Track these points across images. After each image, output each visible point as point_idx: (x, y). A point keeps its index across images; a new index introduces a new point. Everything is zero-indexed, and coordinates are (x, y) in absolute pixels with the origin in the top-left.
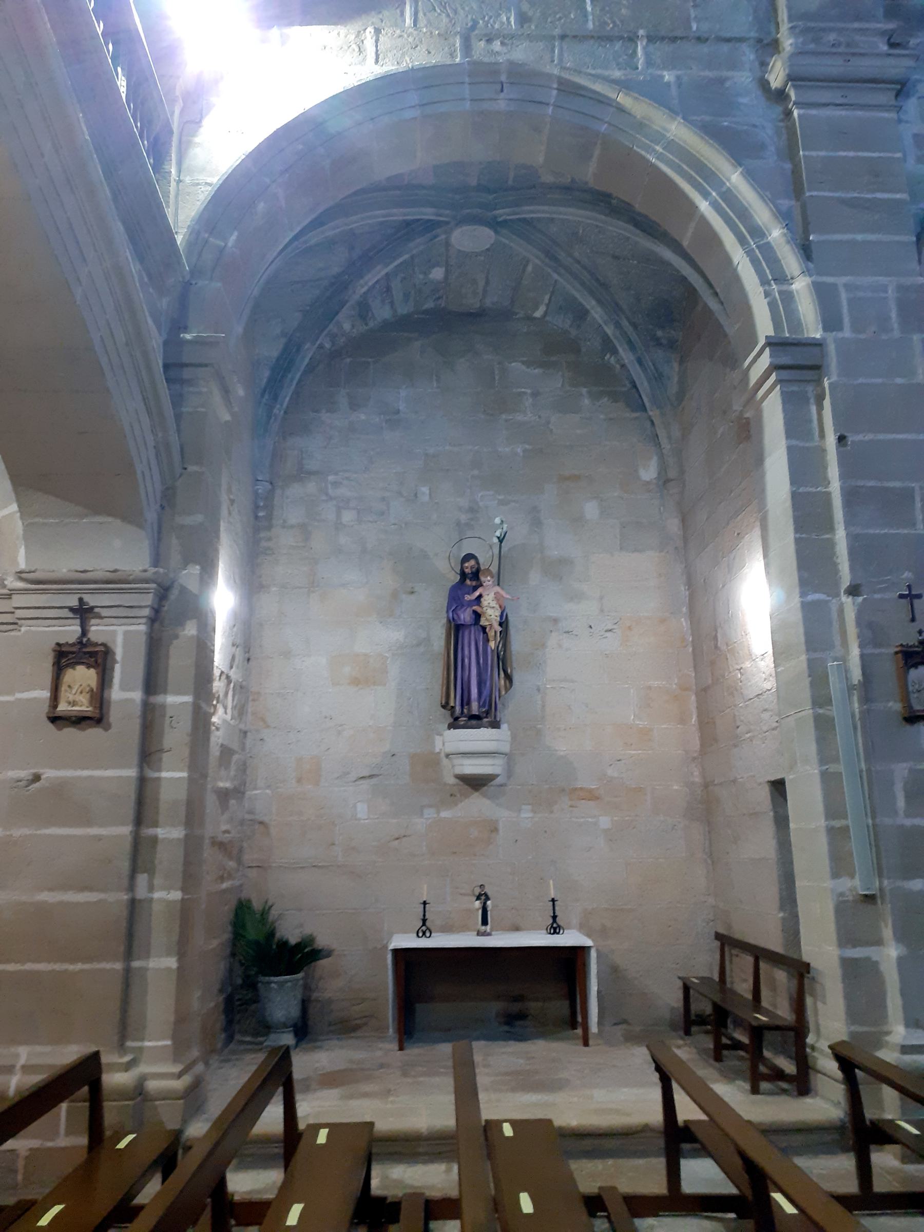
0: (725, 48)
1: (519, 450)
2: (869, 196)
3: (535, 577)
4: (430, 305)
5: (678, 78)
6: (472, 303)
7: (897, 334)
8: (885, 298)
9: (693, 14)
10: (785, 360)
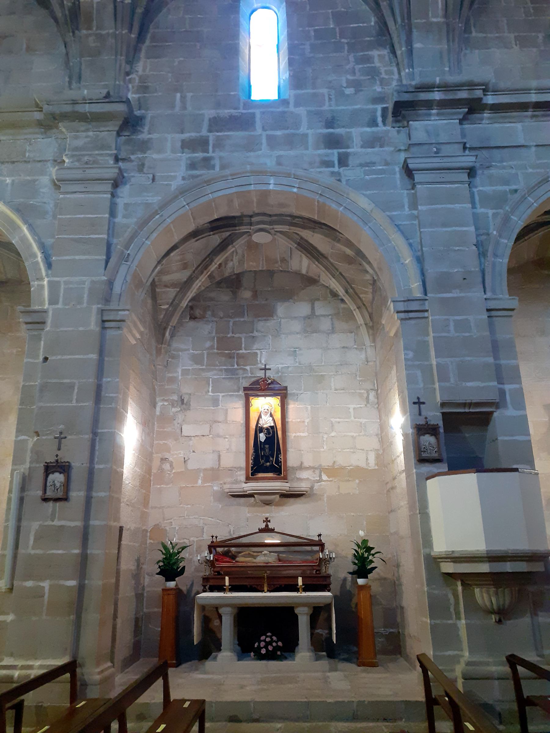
0: (39, 165)
2: (87, 237)
5: (13, 181)
7: (85, 305)
9: (28, 148)
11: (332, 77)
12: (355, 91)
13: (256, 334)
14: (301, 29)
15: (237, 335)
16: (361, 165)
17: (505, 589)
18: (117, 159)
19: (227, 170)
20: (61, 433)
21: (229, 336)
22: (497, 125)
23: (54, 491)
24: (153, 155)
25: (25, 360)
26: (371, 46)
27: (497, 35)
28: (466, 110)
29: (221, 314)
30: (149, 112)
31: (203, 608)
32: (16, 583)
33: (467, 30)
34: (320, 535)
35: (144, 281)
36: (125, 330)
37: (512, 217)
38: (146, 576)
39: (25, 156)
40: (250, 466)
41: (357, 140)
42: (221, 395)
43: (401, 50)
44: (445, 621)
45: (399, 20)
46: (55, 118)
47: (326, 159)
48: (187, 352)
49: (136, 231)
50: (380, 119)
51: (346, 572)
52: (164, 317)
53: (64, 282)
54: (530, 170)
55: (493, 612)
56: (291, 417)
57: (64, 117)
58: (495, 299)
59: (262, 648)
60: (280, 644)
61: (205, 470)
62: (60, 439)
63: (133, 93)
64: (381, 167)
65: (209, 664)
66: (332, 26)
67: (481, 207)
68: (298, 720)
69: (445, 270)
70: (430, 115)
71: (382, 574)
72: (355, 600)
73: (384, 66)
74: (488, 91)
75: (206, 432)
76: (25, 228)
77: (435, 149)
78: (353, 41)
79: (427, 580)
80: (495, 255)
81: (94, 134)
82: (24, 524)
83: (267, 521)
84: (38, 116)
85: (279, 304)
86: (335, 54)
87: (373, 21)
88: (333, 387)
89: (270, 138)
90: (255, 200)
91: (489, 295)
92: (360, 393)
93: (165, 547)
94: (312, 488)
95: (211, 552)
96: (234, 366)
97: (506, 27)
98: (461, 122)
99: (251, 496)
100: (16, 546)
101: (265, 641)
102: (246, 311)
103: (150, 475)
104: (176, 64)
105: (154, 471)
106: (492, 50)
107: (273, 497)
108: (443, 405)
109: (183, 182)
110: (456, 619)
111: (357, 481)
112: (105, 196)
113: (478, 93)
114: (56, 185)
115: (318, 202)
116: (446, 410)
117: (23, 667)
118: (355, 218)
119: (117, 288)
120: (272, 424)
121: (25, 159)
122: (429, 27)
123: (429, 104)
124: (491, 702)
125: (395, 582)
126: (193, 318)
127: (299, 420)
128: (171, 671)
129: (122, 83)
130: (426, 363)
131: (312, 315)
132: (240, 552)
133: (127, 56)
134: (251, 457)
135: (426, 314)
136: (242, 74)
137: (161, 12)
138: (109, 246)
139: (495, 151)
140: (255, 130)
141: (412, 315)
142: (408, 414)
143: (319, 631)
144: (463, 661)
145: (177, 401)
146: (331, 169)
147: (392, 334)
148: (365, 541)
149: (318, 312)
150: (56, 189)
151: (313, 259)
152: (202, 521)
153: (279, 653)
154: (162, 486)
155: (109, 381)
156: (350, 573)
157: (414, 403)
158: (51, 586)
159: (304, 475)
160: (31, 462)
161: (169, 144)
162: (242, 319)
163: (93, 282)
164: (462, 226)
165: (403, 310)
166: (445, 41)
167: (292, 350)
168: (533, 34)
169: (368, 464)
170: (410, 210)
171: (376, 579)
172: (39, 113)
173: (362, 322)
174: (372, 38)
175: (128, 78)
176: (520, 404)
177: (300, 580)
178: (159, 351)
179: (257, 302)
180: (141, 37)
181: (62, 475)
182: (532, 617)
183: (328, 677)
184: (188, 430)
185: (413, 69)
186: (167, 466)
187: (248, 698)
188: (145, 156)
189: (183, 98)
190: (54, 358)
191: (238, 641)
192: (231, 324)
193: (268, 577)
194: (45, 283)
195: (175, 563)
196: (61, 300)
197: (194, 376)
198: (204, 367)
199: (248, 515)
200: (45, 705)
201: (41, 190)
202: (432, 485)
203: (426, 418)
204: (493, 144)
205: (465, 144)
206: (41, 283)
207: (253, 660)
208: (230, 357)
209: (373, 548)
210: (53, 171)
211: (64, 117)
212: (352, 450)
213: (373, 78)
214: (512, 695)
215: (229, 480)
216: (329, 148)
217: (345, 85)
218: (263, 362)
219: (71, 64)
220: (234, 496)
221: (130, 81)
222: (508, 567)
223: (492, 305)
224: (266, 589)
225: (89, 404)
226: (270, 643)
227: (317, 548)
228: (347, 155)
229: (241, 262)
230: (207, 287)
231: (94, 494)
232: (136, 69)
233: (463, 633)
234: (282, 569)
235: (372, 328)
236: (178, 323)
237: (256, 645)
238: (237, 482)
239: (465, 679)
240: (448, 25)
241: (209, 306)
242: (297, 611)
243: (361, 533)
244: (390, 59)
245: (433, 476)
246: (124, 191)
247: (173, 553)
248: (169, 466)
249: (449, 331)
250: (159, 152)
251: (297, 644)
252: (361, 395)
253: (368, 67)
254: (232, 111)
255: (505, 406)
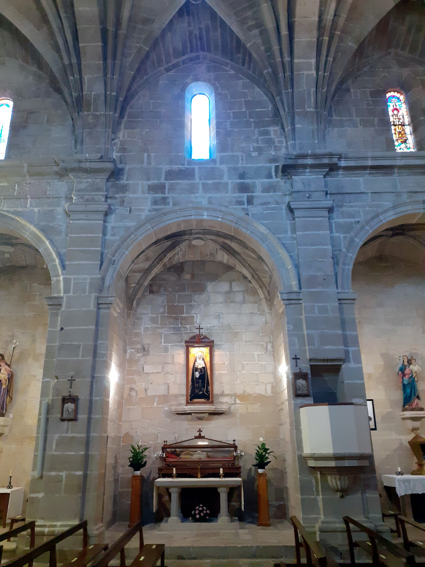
0: (56, 200)
1: (32, 315)
2: (88, 249)
3: (30, 360)
4: (7, 265)
5: (39, 210)
6: (23, 263)
7: (87, 294)
8: (86, 282)
9: (48, 188)
10: (51, 303)
11: (244, 145)
12: (258, 154)
13: (193, 303)
14: (224, 111)
15: (180, 304)
16: (262, 204)
17: (345, 476)
18: (107, 197)
19: (177, 207)
20: (72, 377)
21: (175, 304)
22: (347, 179)
23: (68, 414)
24: (130, 195)
25: (48, 329)
26: (269, 124)
27: (349, 118)
28: (328, 169)
29: (170, 290)
30: (127, 166)
31: (158, 488)
32: (44, 473)
33: (330, 115)
34: (234, 441)
35: (123, 275)
36: (112, 310)
37: (356, 239)
38: (120, 467)
39: (46, 194)
40: (189, 394)
41: (259, 187)
42: (170, 345)
43: (288, 128)
44: (310, 497)
45: (287, 109)
46: (66, 170)
47: (240, 199)
48: (147, 315)
49: (120, 245)
50: (273, 174)
51: (251, 464)
52: (133, 292)
53: (74, 278)
54: (367, 209)
55: (338, 491)
56: (217, 360)
57: (73, 170)
58: (343, 293)
59: (197, 514)
60: (208, 511)
61: (159, 396)
62: (72, 380)
63: (117, 152)
64: (273, 206)
65: (163, 525)
66: (244, 110)
67: (336, 232)
68: (219, 558)
69: (312, 274)
70: (305, 172)
71: (275, 466)
72: (257, 483)
73: (277, 138)
74: (341, 158)
75: (160, 370)
76: (47, 243)
77: (308, 195)
78: (257, 120)
79: (299, 471)
80: (344, 264)
81: (92, 181)
82: (49, 436)
83: (200, 431)
84: (56, 169)
85: (209, 283)
86: (246, 129)
87: (270, 107)
88: (244, 340)
89: (204, 185)
90: (194, 224)
91: (340, 290)
92: (262, 344)
93: (133, 448)
94: (230, 408)
95: (163, 452)
96: (178, 325)
97: (354, 114)
98: (325, 177)
99: (190, 414)
100: (44, 450)
101: (198, 510)
102: (187, 288)
103: (123, 400)
104: (144, 133)
105: (125, 396)
106: (346, 128)
107: (204, 415)
108: (311, 360)
109: (149, 213)
110: (317, 495)
111: (259, 404)
112: (99, 222)
113: (335, 160)
114: (67, 214)
115: (234, 227)
116: (312, 363)
117: (50, 526)
118: (257, 239)
119: (107, 283)
120: (204, 366)
121: (46, 196)
122: (305, 114)
123: (305, 166)
124: (336, 546)
125: (283, 471)
126: (151, 292)
127: (221, 362)
128: (144, 528)
129: (109, 146)
130: (301, 333)
131: (230, 291)
132: (182, 452)
133: (113, 129)
134: (190, 389)
135: (301, 302)
136: (187, 141)
137: (133, 98)
138: (102, 254)
139: (347, 196)
140: (194, 179)
141: (292, 302)
142: (289, 365)
143: (233, 503)
144: (320, 521)
145: (140, 349)
146: (243, 206)
147: (281, 311)
148: (263, 445)
149: (235, 288)
150: (67, 216)
151: (231, 256)
152: (157, 431)
153: (207, 517)
154: (131, 407)
155: (102, 343)
156: (254, 465)
157: (293, 359)
158: (66, 475)
159: (224, 399)
160: (53, 396)
161: (140, 188)
162: (184, 293)
163: (92, 279)
164: (324, 245)
165: (286, 298)
166: (315, 123)
167: (217, 314)
168: (371, 118)
169: (266, 392)
170: (292, 233)
171: (271, 469)
172: (56, 167)
173: (263, 297)
174: (269, 119)
175: (113, 142)
176: (358, 360)
177: (221, 470)
178: (129, 315)
179: (194, 282)
180: (121, 116)
181: (73, 405)
182: (362, 494)
183: (239, 533)
184: (148, 369)
185: (295, 141)
186: (133, 394)
187: (189, 545)
188: (124, 195)
189: (149, 157)
190: (67, 328)
191: (181, 510)
192: (177, 296)
193: (200, 468)
194: (61, 278)
195: (140, 459)
196: (72, 290)
197: (152, 332)
198: (159, 326)
199: (188, 427)
200: (65, 549)
201: (58, 217)
202: (303, 410)
203: (300, 369)
204: (344, 191)
205: (327, 192)
206: (58, 278)
207: (191, 522)
208: (176, 319)
209: (268, 449)
210: (66, 206)
211: (73, 170)
212: (256, 383)
213: (270, 145)
214: (347, 542)
215: (174, 403)
216: (241, 193)
217: (252, 150)
218: (198, 322)
219: (77, 133)
220: (178, 414)
221: (115, 144)
222: (346, 463)
223: (342, 296)
224: (199, 476)
225: (90, 358)
226: (202, 511)
227: (233, 449)
228: (252, 197)
229: (184, 255)
230: (162, 271)
231: (93, 416)
232: (119, 136)
233: (321, 504)
234: (211, 462)
235: (270, 300)
236: (142, 295)
237: (193, 512)
238: (180, 405)
239: (320, 532)
240: (317, 113)
241: (162, 284)
242: (219, 490)
243: (261, 439)
244: (281, 133)
245: (304, 406)
246: (112, 218)
247: (139, 452)
248: (135, 393)
249: (314, 313)
250: (134, 192)
251: (219, 512)
252: (262, 345)
253: (266, 138)
254: (180, 166)
255: (349, 361)
